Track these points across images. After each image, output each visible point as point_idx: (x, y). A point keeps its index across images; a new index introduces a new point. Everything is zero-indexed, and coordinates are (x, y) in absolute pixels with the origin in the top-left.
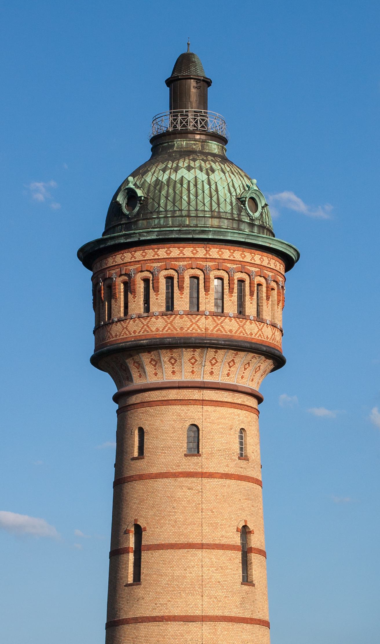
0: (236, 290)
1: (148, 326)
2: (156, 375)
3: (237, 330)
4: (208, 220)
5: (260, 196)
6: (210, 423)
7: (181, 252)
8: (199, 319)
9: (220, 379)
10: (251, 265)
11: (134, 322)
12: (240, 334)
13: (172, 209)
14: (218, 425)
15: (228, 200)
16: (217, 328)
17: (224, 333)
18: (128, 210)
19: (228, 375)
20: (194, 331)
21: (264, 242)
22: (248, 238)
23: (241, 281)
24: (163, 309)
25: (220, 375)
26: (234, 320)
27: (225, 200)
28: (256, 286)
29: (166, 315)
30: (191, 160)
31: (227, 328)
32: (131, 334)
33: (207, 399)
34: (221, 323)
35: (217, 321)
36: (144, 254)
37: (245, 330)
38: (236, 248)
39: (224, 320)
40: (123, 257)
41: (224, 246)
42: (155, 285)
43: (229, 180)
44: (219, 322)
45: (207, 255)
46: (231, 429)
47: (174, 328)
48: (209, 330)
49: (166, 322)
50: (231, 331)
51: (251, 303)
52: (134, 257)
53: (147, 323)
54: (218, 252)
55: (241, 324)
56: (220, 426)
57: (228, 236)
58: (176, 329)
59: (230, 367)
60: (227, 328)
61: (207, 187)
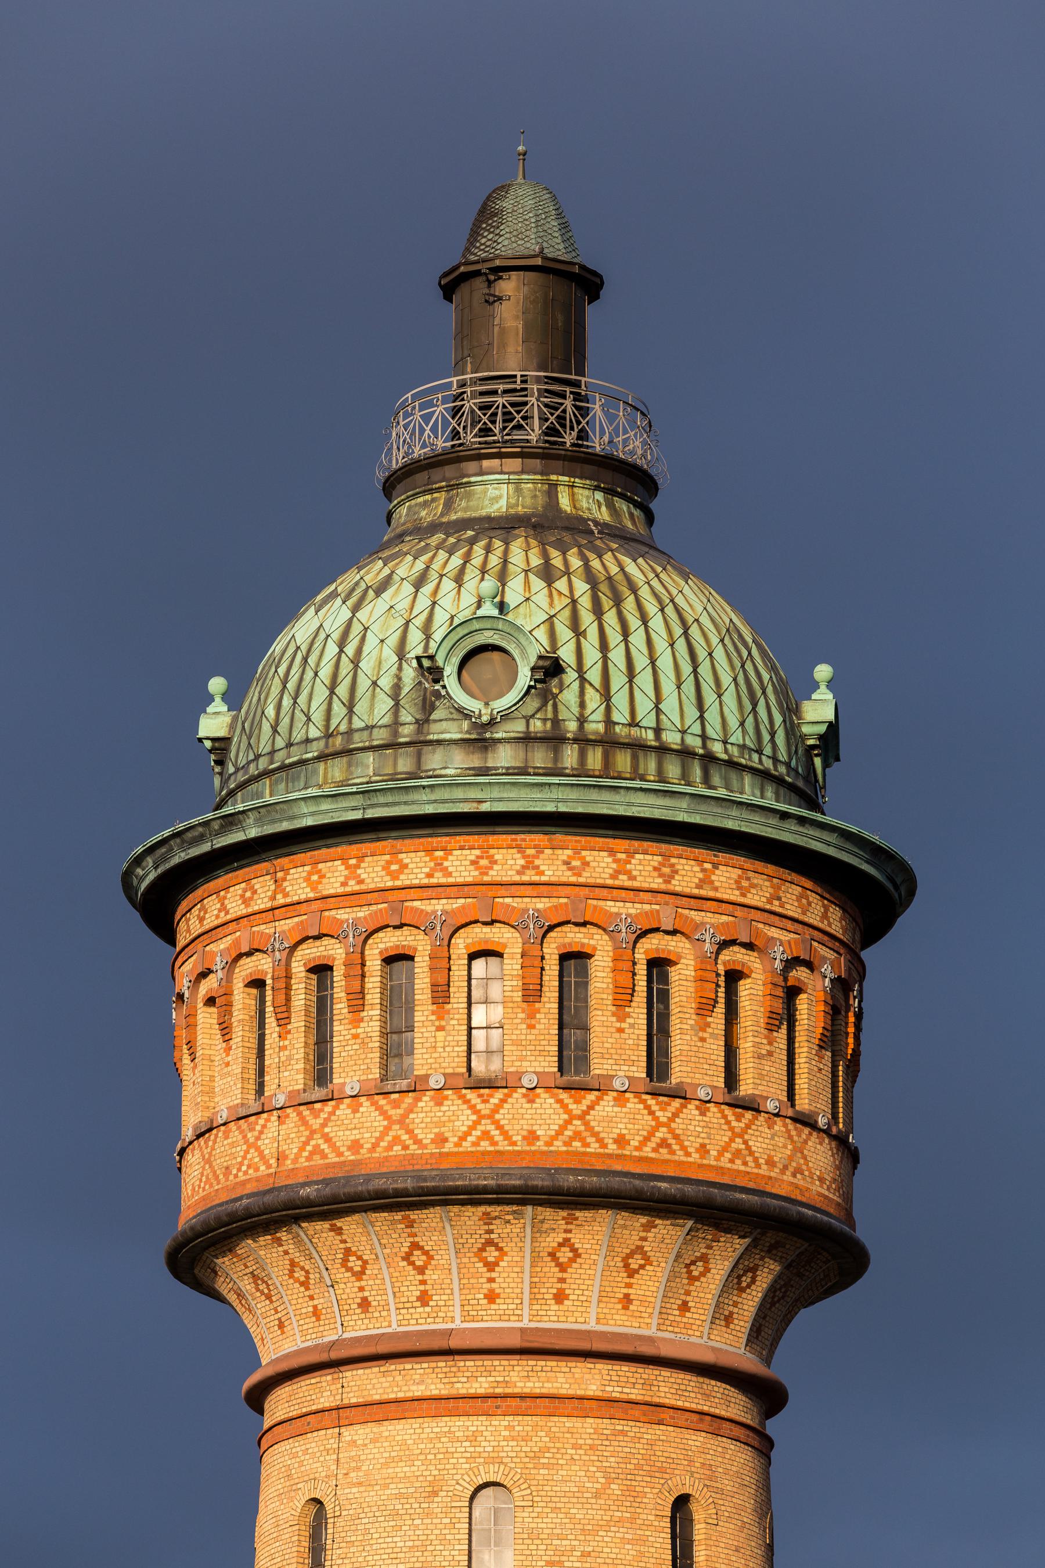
3: (380, 1139)
4: (315, 772)
5: (516, 634)
6: (360, 1484)
8: (264, 1126)
9: (395, 1320)
10: (429, 892)
12: (390, 1148)
14: (386, 1486)
15: (386, 682)
16: (389, 1138)
19: (424, 1299)
21: (444, 801)
22: (373, 806)
25: (392, 1307)
26: (367, 1104)
27: (375, 683)
30: (551, 544)
31: (343, 1137)
32: (604, 1146)
33: (354, 1401)
34: (324, 1125)
35: (312, 1121)
37: (410, 1132)
38: (365, 848)
39: (333, 1113)
41: (324, 851)
42: (625, 980)
44: (316, 1123)
45: (438, 874)
46: (435, 1494)
48: (286, 1157)
50: (355, 1146)
51: (440, 1028)
54: (307, 879)
55: (576, 1109)
56: (392, 1490)
57: (304, 816)
60: (343, 1137)
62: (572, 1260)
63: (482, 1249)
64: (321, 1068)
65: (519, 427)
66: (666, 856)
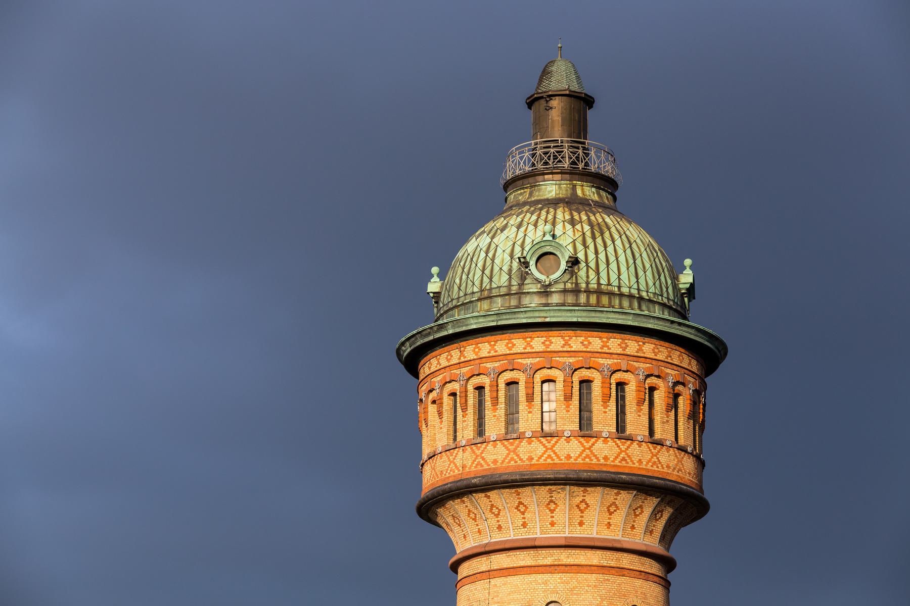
0: (502, 399)
3: (505, 459)
4: (476, 306)
9: (512, 534)
12: (509, 462)
17: (486, 467)
19: (524, 525)
23: (511, 383)
24: (576, 427)
31: (490, 458)
32: (599, 460)
36: (547, 343)
37: (518, 456)
42: (607, 391)
43: (600, 220)
44: (478, 452)
51: (530, 412)
55: (512, 448)
59: (523, 513)
61: (483, 255)
62: (586, 508)
63: (548, 504)
64: (480, 430)
65: (560, 161)
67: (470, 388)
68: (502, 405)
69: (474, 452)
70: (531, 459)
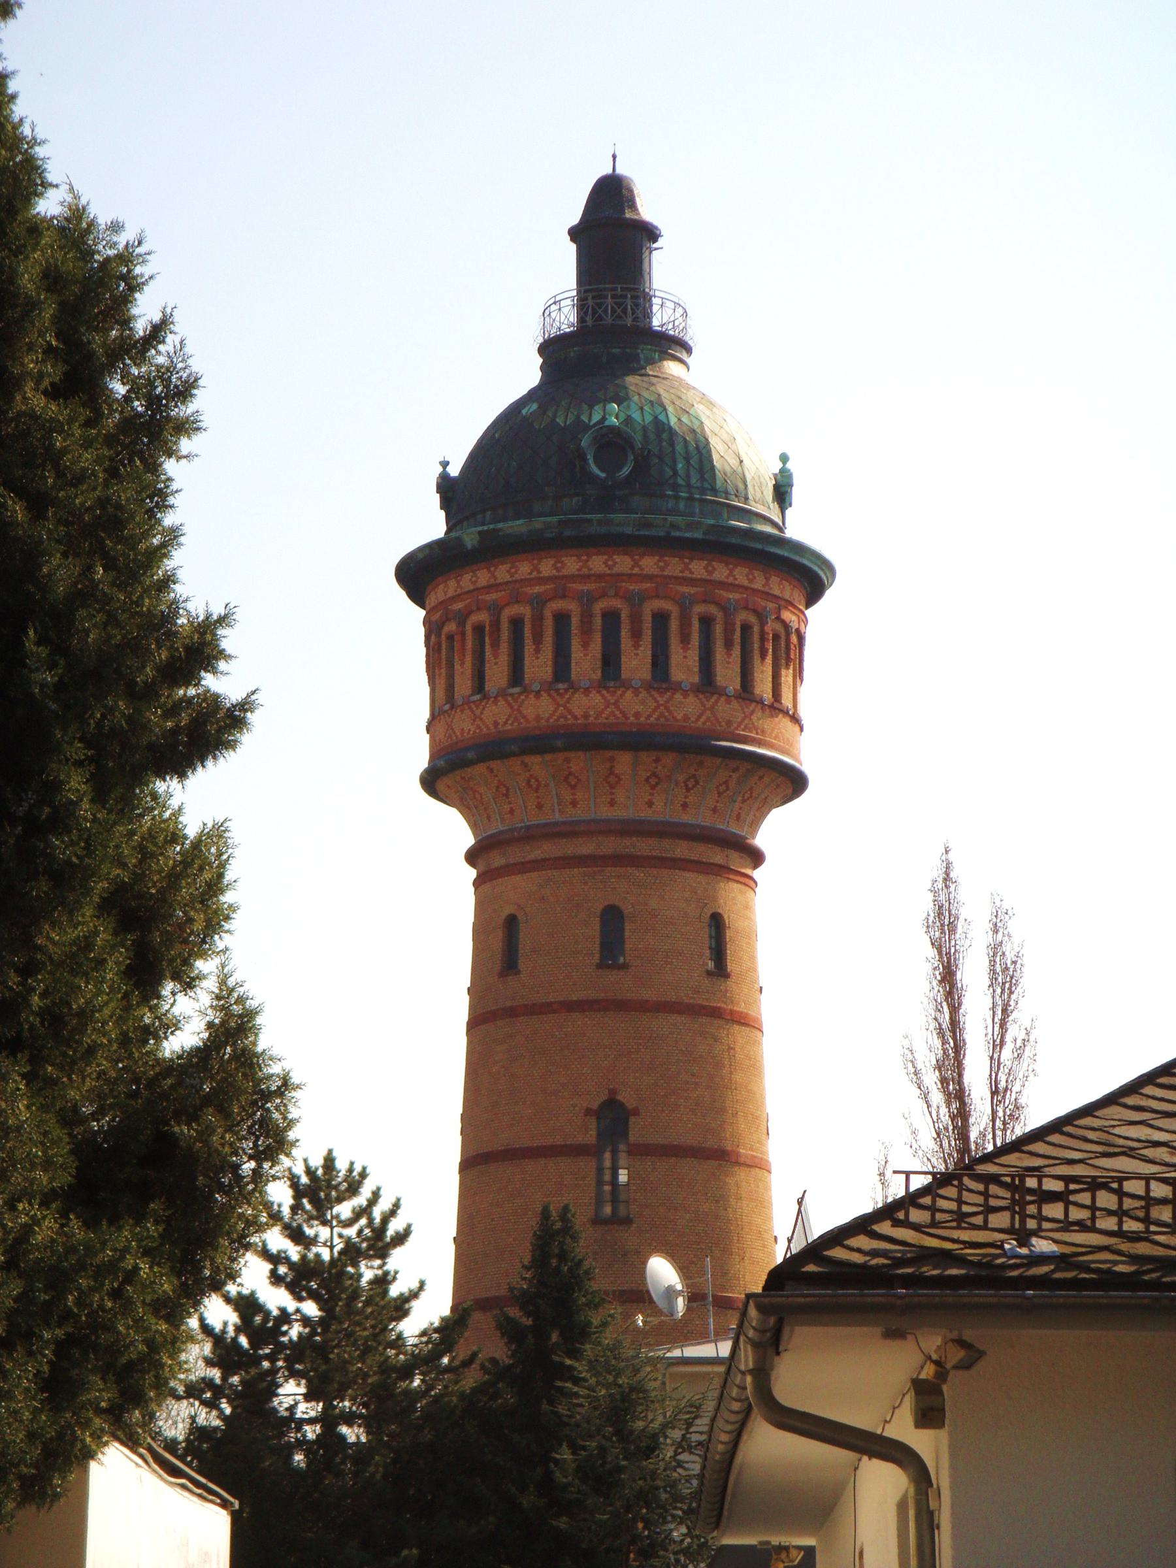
1: (667, 708)
2: (650, 806)
7: (731, 574)
11: (637, 695)
12: (658, 719)
13: (699, 484)
18: (602, 470)
20: (662, 720)
24: (696, 679)
28: (738, 629)
29: (703, 693)
32: (627, 718)
36: (661, 564)
40: (610, 563)
47: (717, 719)
49: (704, 705)
52: (639, 566)
53: (667, 702)
55: (661, 701)
58: (720, 723)
62: (617, 783)
63: (607, 777)
64: (516, 675)
65: (619, 317)
66: (662, 556)
67: (548, 614)
68: (597, 638)
69: (473, 712)
70: (586, 716)
